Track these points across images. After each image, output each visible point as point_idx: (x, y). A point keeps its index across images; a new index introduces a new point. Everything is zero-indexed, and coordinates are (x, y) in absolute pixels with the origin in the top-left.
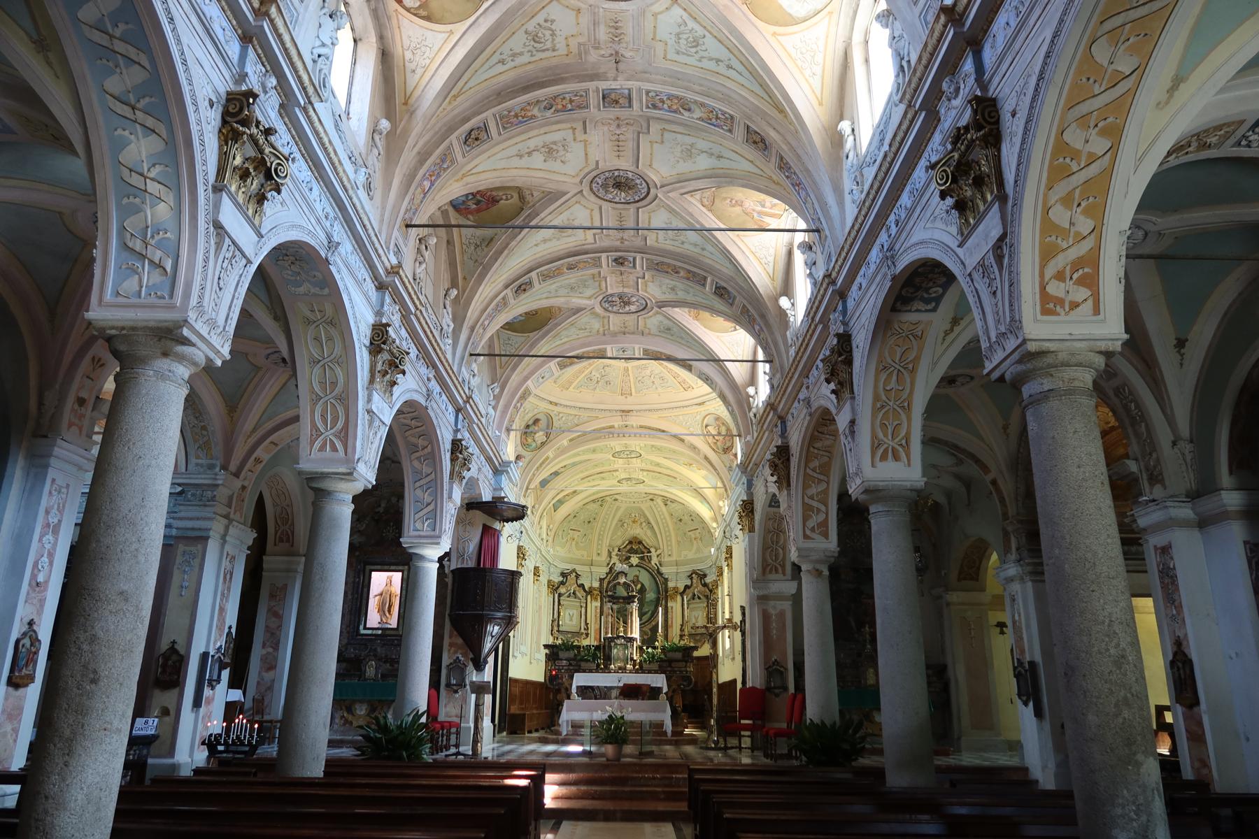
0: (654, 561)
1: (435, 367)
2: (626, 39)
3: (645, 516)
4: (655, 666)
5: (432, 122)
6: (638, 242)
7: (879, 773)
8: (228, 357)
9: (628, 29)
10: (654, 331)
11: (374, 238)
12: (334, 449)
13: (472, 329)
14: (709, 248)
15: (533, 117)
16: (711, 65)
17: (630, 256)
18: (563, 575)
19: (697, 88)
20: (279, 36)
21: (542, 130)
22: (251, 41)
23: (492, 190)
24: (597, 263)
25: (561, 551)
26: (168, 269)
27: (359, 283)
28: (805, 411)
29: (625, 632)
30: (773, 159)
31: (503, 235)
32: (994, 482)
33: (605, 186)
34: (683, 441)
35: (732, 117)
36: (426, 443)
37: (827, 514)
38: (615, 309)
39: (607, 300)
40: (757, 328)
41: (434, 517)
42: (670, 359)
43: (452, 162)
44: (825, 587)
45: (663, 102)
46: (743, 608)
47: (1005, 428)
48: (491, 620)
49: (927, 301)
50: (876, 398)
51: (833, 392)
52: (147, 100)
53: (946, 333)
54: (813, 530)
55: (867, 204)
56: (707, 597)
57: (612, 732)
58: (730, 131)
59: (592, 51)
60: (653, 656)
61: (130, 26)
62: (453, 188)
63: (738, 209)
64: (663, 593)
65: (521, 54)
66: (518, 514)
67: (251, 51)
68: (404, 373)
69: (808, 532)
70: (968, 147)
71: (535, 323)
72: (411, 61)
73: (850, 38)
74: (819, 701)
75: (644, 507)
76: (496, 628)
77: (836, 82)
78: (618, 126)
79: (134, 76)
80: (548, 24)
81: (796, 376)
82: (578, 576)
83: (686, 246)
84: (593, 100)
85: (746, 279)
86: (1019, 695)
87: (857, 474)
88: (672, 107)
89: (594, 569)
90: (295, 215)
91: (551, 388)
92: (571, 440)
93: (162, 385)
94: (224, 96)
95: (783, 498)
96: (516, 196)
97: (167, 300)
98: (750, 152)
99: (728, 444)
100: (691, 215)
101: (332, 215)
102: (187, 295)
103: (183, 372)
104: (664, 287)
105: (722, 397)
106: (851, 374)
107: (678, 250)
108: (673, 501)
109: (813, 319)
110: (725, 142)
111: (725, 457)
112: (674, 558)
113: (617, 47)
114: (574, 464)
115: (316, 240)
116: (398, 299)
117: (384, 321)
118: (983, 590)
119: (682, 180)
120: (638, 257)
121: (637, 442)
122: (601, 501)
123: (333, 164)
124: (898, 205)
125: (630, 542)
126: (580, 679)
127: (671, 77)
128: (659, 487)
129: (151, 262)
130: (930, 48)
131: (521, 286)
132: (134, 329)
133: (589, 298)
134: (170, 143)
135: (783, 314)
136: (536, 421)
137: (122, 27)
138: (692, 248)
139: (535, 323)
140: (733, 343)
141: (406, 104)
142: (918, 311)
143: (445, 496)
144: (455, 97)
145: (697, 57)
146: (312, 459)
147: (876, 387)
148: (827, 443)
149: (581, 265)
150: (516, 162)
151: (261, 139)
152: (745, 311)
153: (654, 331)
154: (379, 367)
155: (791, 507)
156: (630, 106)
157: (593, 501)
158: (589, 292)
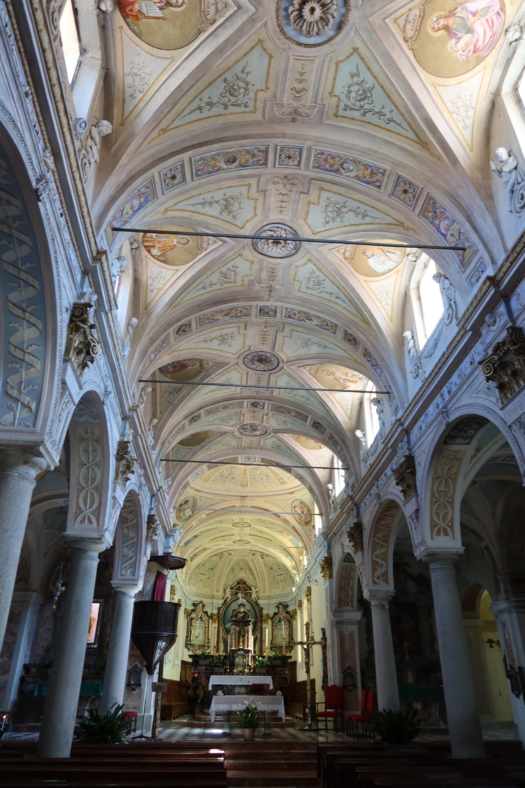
0: (254, 596)
1: (145, 468)
2: (278, 279)
3: (248, 565)
4: (264, 670)
5: (161, 320)
6: (267, 393)
7: (446, 748)
8: (58, 464)
9: (280, 274)
10: (269, 447)
11: (127, 389)
12: (90, 522)
13: (163, 444)
14: (312, 399)
15: (217, 320)
16: (327, 296)
17: (261, 402)
18: (194, 605)
19: (316, 308)
20: (103, 272)
21: (220, 327)
22: (88, 274)
23: (184, 360)
24: (241, 405)
25: (194, 589)
26: (33, 407)
27: (115, 416)
28: (375, 501)
29: (244, 647)
30: (360, 350)
31: (187, 388)
32: (487, 548)
33: (252, 361)
34: (279, 516)
35: (336, 325)
36: (133, 517)
37: (387, 568)
38: (247, 433)
39: (243, 428)
40: (339, 448)
41: (134, 566)
42: (278, 465)
43: (168, 344)
44: (386, 615)
45: (295, 314)
46: (323, 630)
47: (493, 513)
48: (160, 638)
49: (465, 438)
50: (433, 496)
51: (402, 491)
52: (34, 307)
53: (473, 457)
54: (378, 578)
55: (429, 380)
56: (289, 621)
57: (249, 719)
58: (334, 333)
59: (256, 284)
60: (263, 663)
61: (32, 265)
62: (165, 359)
63: (331, 377)
64: (259, 619)
65: (216, 284)
66: (180, 564)
67: (87, 280)
68: (133, 472)
69: (376, 580)
70: (504, 354)
71: (196, 441)
72: (151, 285)
73: (409, 285)
74: (386, 694)
75: (248, 559)
76: (164, 643)
77: (400, 310)
78: (266, 327)
79: (29, 293)
80: (234, 269)
81: (370, 479)
82: (203, 606)
83: (297, 397)
84: (254, 311)
85: (334, 418)
86: (513, 690)
87: (421, 544)
88: (299, 318)
89: (214, 601)
90: (95, 378)
91: (202, 482)
92: (207, 515)
93: (22, 482)
94: (72, 305)
95: (358, 558)
96: (198, 364)
97: (31, 428)
98: (346, 346)
99: (309, 519)
100: (303, 379)
101: (108, 375)
102: (44, 426)
103: (33, 473)
104: (279, 421)
105: (311, 490)
106: (415, 480)
107: (291, 399)
108: (267, 556)
109: (386, 445)
110: (329, 339)
111: (306, 527)
112: (267, 594)
113: (271, 283)
114: (207, 531)
115: (100, 391)
116: (133, 426)
117: (125, 440)
118: (478, 617)
119: (300, 359)
120: (267, 402)
121: (249, 517)
122: (220, 555)
123: (114, 345)
124: (450, 381)
125: (238, 583)
126: (215, 680)
127: (301, 301)
128: (260, 546)
129: (23, 404)
130: (478, 298)
131: (194, 418)
132: (8, 446)
133: (232, 426)
134: (44, 333)
135: (357, 441)
136: (186, 502)
137: (28, 265)
138: (301, 399)
139: (196, 441)
140: (319, 456)
141: (146, 309)
142: (459, 444)
143: (143, 552)
144: (175, 306)
145: (319, 291)
146: (74, 529)
147: (432, 489)
148: (388, 522)
149: (231, 406)
150: (203, 345)
151: (88, 330)
152: (331, 437)
153: (269, 447)
154: (121, 469)
155: (363, 563)
156: (275, 316)
157: (216, 555)
158: (232, 423)
